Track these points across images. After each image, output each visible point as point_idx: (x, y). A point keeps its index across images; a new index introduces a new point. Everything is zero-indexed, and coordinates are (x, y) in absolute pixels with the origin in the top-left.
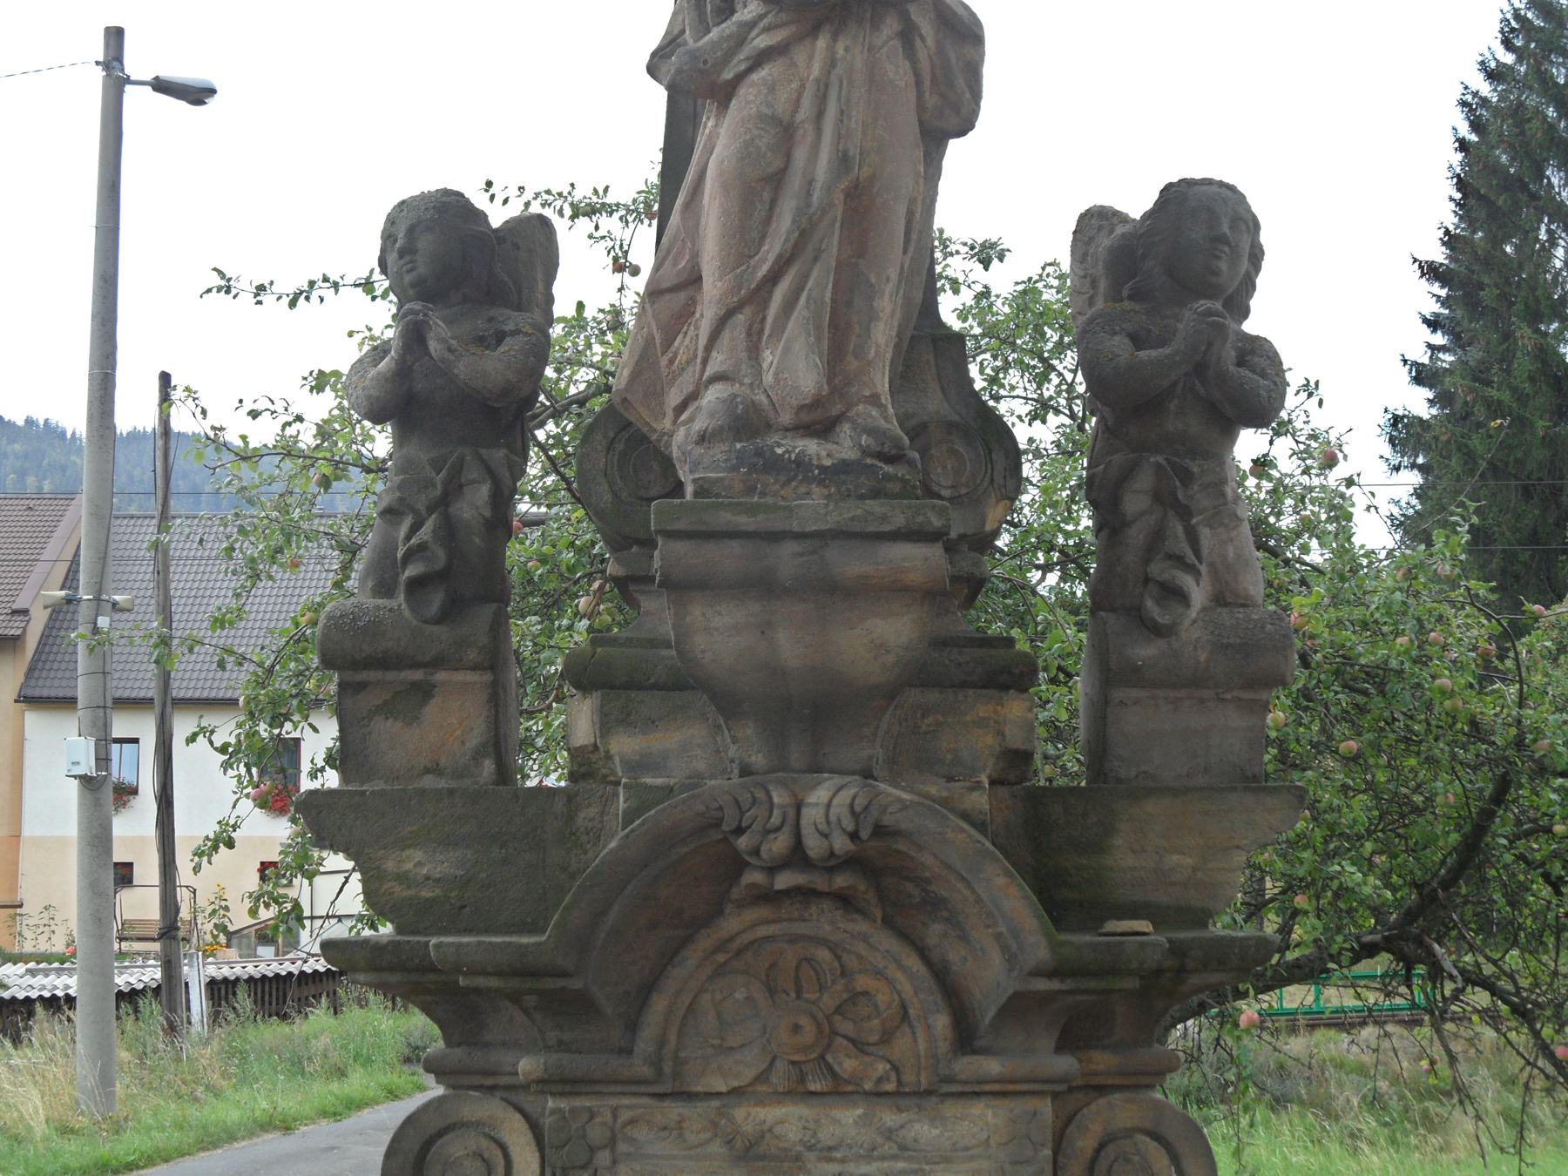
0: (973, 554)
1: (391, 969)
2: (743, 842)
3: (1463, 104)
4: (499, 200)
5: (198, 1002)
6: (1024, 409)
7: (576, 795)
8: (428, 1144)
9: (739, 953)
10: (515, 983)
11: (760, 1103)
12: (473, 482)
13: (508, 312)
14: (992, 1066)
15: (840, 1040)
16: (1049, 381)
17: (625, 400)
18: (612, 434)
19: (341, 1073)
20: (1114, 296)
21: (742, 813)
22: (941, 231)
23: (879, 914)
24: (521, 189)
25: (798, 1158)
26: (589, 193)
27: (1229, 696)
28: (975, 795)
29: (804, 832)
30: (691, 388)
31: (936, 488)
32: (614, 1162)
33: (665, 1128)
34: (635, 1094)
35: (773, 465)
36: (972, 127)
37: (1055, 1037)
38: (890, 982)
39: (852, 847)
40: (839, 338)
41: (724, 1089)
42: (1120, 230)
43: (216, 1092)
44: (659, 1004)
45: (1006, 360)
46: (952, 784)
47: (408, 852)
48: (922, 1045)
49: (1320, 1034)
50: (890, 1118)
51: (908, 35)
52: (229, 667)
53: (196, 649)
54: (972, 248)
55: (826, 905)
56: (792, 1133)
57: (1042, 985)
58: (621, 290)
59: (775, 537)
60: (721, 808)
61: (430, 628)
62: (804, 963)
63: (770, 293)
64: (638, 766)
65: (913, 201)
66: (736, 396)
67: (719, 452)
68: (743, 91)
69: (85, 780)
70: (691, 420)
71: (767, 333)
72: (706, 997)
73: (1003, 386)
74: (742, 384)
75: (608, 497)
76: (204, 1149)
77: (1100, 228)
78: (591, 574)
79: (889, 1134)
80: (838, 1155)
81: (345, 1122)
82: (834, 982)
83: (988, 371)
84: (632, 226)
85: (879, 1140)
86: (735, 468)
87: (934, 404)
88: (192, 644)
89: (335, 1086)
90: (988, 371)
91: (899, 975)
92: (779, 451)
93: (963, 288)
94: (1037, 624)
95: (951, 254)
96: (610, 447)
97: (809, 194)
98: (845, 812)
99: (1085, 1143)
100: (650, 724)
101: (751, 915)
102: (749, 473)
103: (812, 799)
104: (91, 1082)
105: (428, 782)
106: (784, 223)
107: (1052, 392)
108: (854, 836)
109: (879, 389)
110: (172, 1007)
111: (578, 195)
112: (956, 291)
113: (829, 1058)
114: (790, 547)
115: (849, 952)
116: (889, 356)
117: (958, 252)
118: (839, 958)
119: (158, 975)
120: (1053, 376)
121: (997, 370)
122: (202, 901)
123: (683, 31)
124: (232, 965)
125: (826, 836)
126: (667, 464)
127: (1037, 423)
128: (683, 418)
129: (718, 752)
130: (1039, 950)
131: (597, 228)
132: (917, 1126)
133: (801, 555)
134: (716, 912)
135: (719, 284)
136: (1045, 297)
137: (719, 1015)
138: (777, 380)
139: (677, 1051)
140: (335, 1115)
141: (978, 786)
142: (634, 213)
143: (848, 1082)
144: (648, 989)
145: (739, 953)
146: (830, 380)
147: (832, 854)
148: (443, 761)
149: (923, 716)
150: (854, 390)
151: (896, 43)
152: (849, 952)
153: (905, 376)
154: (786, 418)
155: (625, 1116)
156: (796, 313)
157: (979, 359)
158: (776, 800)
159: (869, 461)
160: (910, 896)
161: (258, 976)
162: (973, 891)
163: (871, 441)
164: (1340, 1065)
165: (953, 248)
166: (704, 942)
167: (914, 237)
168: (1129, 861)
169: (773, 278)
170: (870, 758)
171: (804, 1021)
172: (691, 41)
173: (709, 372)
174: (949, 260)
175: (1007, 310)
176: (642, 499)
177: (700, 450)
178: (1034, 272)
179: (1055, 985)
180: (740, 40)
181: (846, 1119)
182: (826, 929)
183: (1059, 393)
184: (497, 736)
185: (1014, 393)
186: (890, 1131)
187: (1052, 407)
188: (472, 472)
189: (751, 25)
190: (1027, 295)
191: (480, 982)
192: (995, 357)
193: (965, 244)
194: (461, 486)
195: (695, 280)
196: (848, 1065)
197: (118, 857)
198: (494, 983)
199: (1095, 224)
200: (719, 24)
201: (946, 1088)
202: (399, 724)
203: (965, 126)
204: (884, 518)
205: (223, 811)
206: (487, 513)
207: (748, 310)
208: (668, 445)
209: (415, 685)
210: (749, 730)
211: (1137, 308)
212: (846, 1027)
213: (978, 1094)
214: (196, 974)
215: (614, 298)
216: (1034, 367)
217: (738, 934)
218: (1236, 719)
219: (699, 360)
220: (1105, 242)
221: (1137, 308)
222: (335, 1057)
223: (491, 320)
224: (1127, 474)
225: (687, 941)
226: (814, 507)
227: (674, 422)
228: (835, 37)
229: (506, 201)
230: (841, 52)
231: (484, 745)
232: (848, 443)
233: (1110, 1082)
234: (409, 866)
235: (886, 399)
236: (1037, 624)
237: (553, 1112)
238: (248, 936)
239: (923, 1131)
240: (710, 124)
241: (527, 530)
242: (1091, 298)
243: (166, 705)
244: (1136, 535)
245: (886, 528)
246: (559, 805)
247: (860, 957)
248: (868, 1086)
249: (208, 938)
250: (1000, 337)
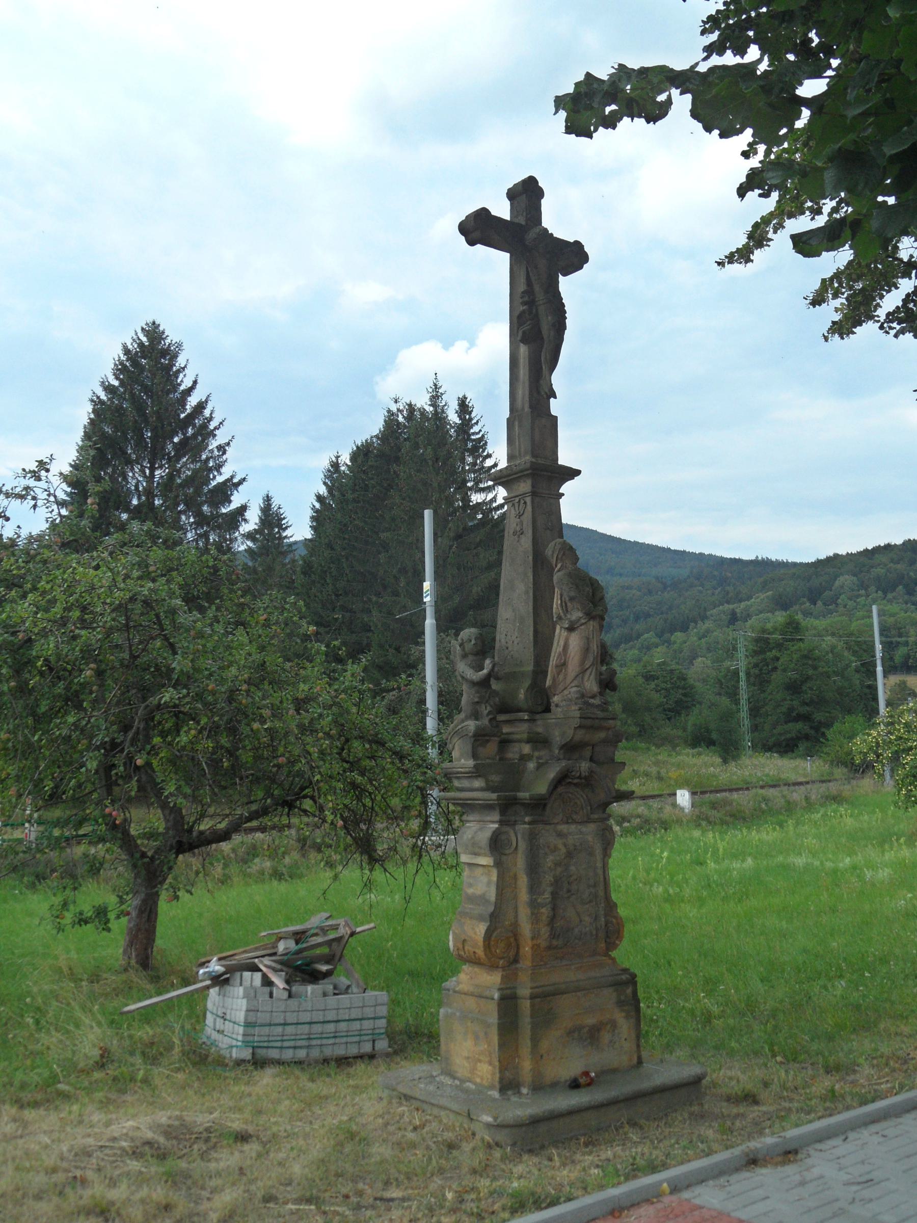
3: (92, 401)
50: (579, 827)
56: (565, 831)
239: (584, 829)
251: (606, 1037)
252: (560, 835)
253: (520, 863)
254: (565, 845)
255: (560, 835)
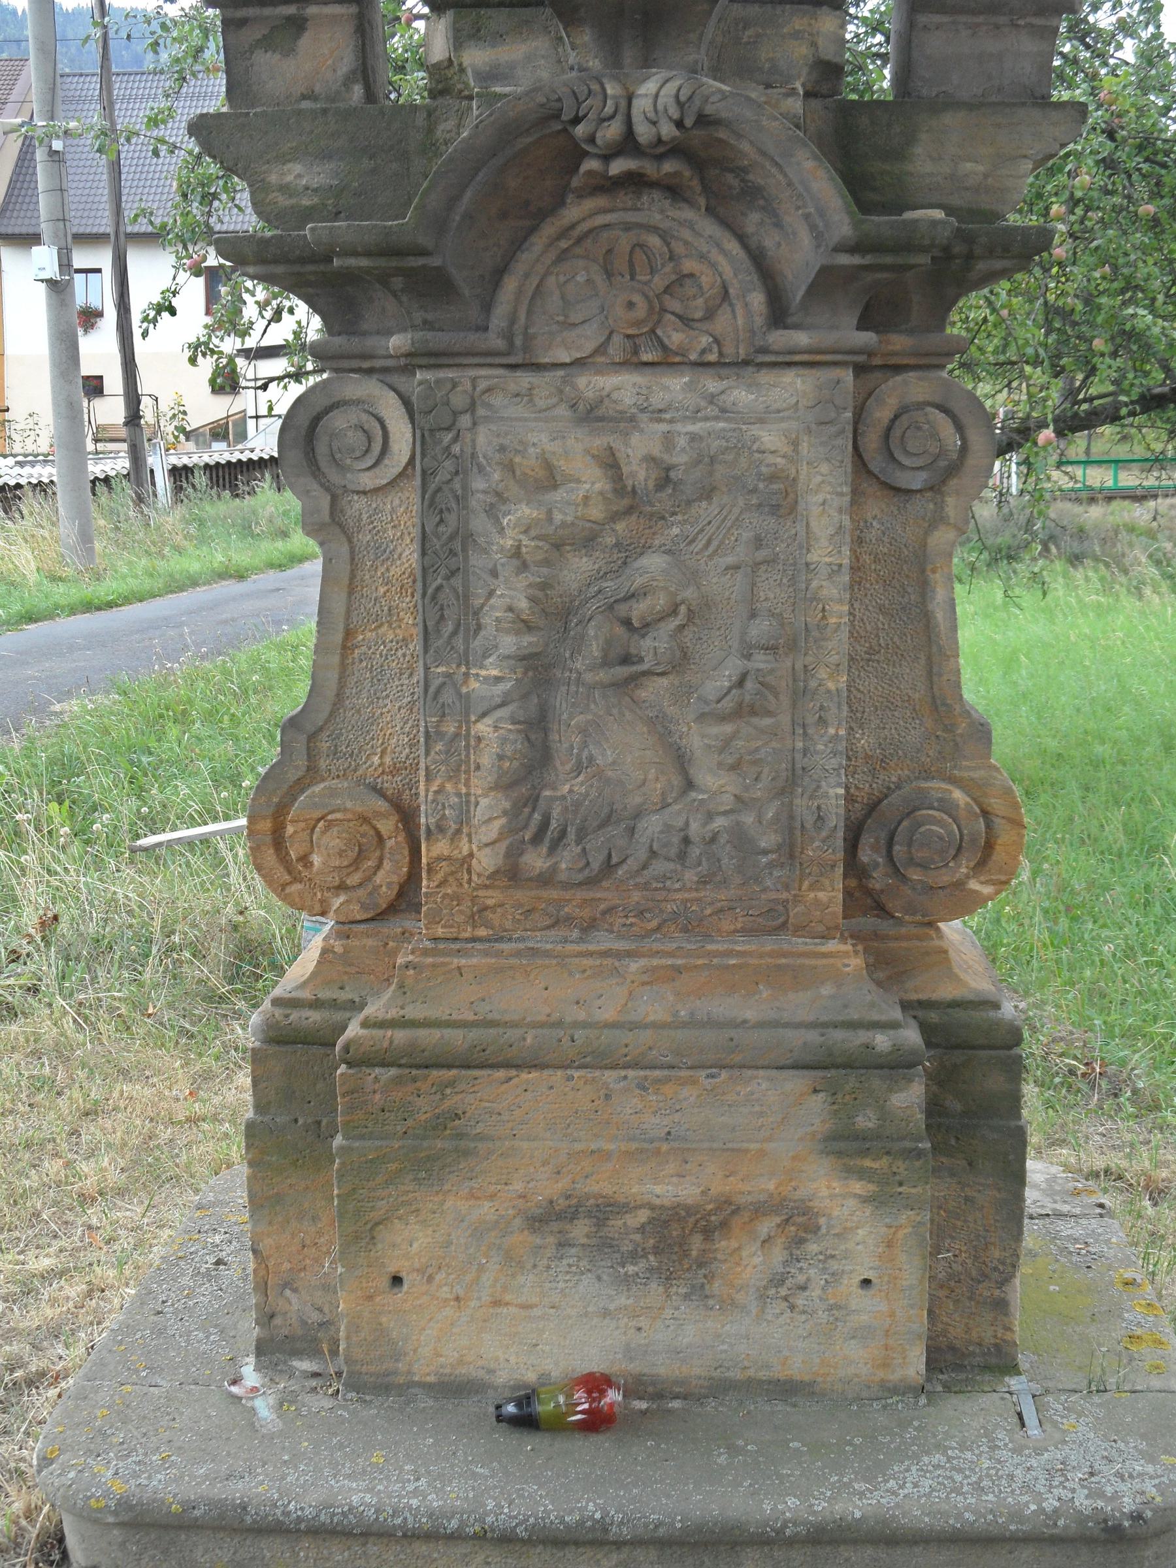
1: (276, 261)
2: (580, 130)
5: (162, 482)
7: (435, 109)
8: (317, 420)
9: (579, 240)
10: (382, 262)
11: (599, 372)
14: (802, 338)
15: (669, 316)
19: (285, 534)
21: (579, 104)
23: (702, 201)
25: (632, 419)
27: (1021, 22)
28: (790, 101)
29: (634, 120)
32: (475, 424)
33: (517, 395)
34: (491, 365)
37: (857, 313)
38: (713, 265)
39: (677, 133)
41: (568, 360)
43: (179, 550)
44: (510, 285)
46: (769, 91)
47: (290, 165)
48: (740, 321)
49: (1116, 505)
50: (712, 385)
52: (162, 154)
53: (133, 141)
55: (656, 194)
57: (845, 259)
60: (559, 100)
62: (637, 249)
64: (490, 75)
69: (51, 283)
72: (551, 280)
76: (172, 592)
79: (712, 399)
80: (668, 416)
81: (289, 572)
82: (663, 265)
85: (703, 404)
88: (131, 135)
89: (280, 544)
91: (721, 259)
98: (671, 101)
99: (882, 414)
100: (498, 37)
101: (590, 204)
103: (642, 90)
104: (73, 540)
105: (306, 105)
108: (679, 124)
110: (139, 483)
113: (659, 332)
115: (678, 239)
118: (668, 244)
119: (127, 465)
122: (164, 406)
124: (192, 455)
125: (654, 123)
129: (559, 62)
130: (842, 226)
132: (736, 392)
134: (559, 202)
137: (563, 298)
139: (526, 328)
140: (280, 567)
141: (793, 92)
143: (677, 354)
144: (499, 273)
145: (579, 240)
147: (660, 141)
148: (317, 89)
149: (744, 28)
152: (678, 239)
155: (482, 385)
158: (609, 91)
160: (730, 188)
161: (212, 463)
162: (786, 175)
164: (1131, 529)
166: (549, 229)
168: (928, 168)
170: (696, 62)
171: (637, 298)
179: (856, 260)
181: (674, 387)
182: (656, 218)
184: (364, 64)
186: (713, 396)
191: (352, 262)
196: (675, 338)
197: (86, 371)
198: (364, 262)
201: (761, 358)
202: (277, 56)
205: (167, 283)
209: (289, 19)
210: (586, 36)
212: (675, 305)
213: (789, 364)
214: (158, 463)
217: (578, 222)
218: (1029, 45)
222: (279, 522)
225: (533, 230)
231: (354, 72)
233: (905, 362)
234: (289, 178)
237: (420, 383)
238: (203, 435)
239: (741, 396)
243: (122, 242)
246: (420, 120)
247: (686, 243)
248: (693, 357)
249: (171, 438)
251: (750, 1260)
252: (591, 415)
253: (397, 521)
254: (611, 464)
255: (591, 415)
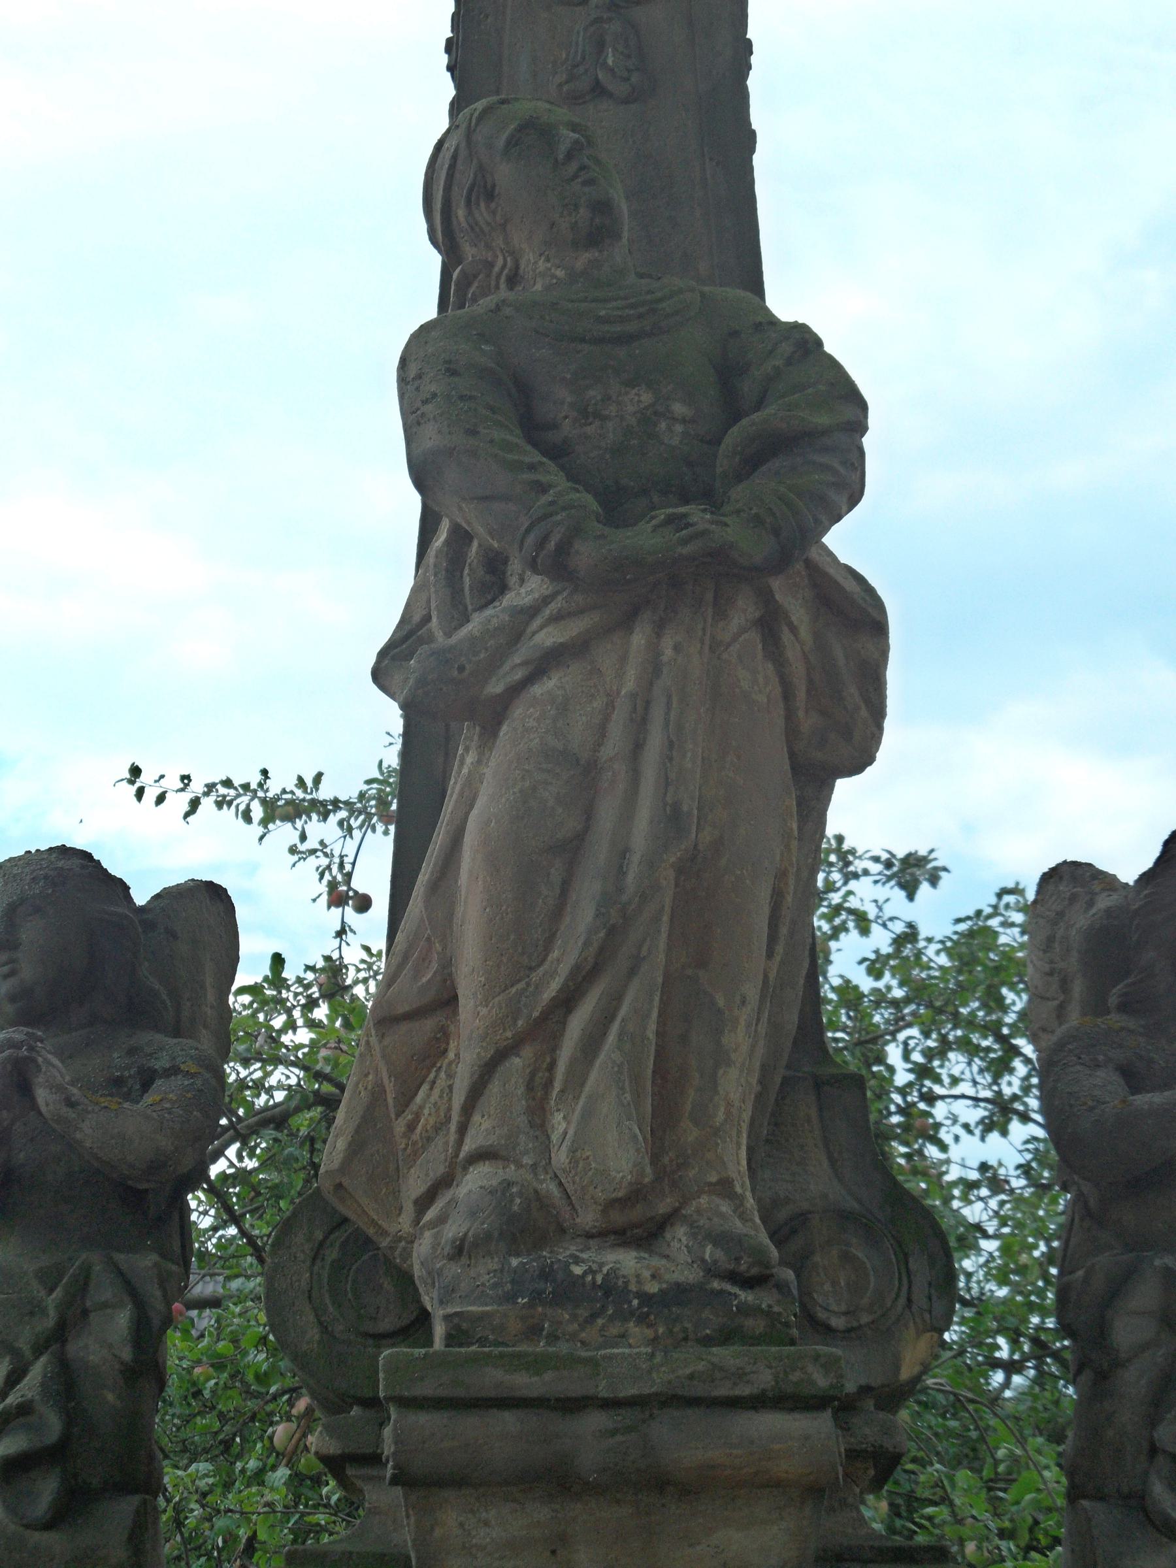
0: (881, 1415)
4: (151, 795)
6: (974, 1115)
12: (105, 1305)
13: (159, 1037)
16: (1011, 1071)
17: (340, 1186)
18: (319, 1235)
20: (1096, 1006)
22: (840, 839)
24: (186, 779)
26: (291, 785)
30: (442, 1169)
31: (821, 1315)
35: (565, 1291)
36: (870, 760)
40: (667, 1094)
42: (1104, 902)
45: (943, 1039)
51: (770, 623)
54: (888, 864)
58: (341, 933)
59: (571, 1406)
61: (37, 1537)
63: (563, 1023)
65: (782, 875)
66: (510, 1184)
67: (484, 1270)
68: (518, 711)
70: (442, 1220)
71: (557, 1085)
73: (938, 1080)
74: (519, 1165)
75: (314, 1334)
77: (1073, 898)
78: (292, 1390)
83: (917, 1057)
84: (357, 834)
86: (510, 1298)
87: (818, 1182)
90: (917, 1057)
92: (578, 1270)
93: (875, 927)
94: (997, 1463)
95: (856, 876)
96: (317, 1255)
97: (621, 872)
102: (531, 1305)
106: (583, 917)
107: (1016, 1089)
109: (732, 1172)
111: (274, 788)
112: (865, 931)
114: (596, 1420)
116: (746, 1116)
117: (866, 872)
120: (1017, 1064)
121: (929, 1054)
123: (427, 619)
126: (405, 1280)
127: (994, 1136)
128: (430, 1215)
131: (303, 837)
133: (613, 1433)
135: (484, 1011)
136: (1003, 939)
138: (574, 1161)
142: (356, 812)
146: (655, 1159)
150: (691, 1173)
151: (754, 636)
153: (772, 1139)
154: (588, 1218)
156: (602, 1057)
157: (901, 1036)
159: (716, 1285)
163: (719, 1254)
165: (858, 865)
167: (784, 930)
169: (567, 1001)
172: (439, 635)
173: (468, 1147)
174: (853, 885)
175: (943, 960)
176: (367, 1335)
177: (455, 1269)
178: (985, 901)
180: (515, 631)
183: (1026, 1089)
185: (957, 1091)
187: (1016, 1112)
188: (104, 1290)
189: (532, 611)
190: (973, 940)
192: (926, 1035)
193: (876, 859)
194: (85, 1313)
195: (448, 1001)
199: (1070, 880)
200: (482, 608)
203: (860, 758)
204: (740, 1376)
206: (127, 1354)
207: (528, 1052)
208: (407, 1254)
211: (1132, 1025)
215: (330, 946)
216: (988, 1050)
219: (453, 1127)
220: (1081, 920)
221: (1132, 1025)
223: (132, 1051)
224: (1118, 1287)
226: (631, 1357)
227: (417, 1221)
228: (660, 628)
229: (161, 799)
230: (668, 653)
232: (684, 1257)
235: (742, 1186)
236: (997, 1463)
240: (469, 759)
241: (194, 1313)
242: (1061, 1007)
244: (1135, 1381)
245: (745, 1390)
250: (932, 1003)
